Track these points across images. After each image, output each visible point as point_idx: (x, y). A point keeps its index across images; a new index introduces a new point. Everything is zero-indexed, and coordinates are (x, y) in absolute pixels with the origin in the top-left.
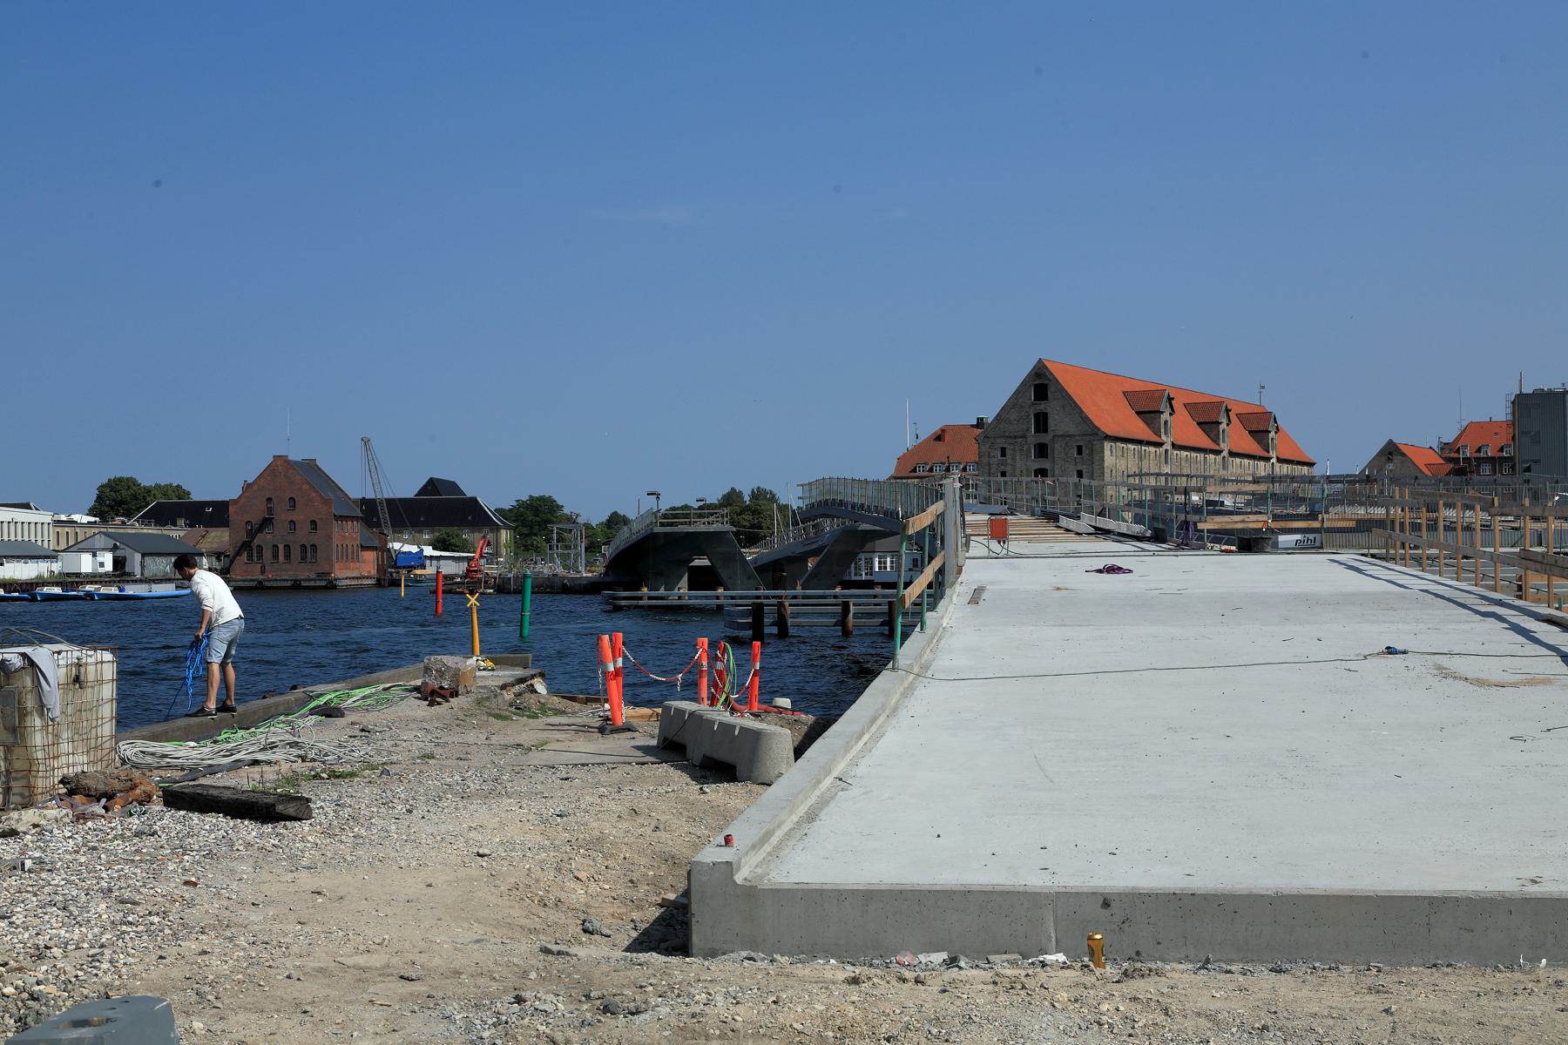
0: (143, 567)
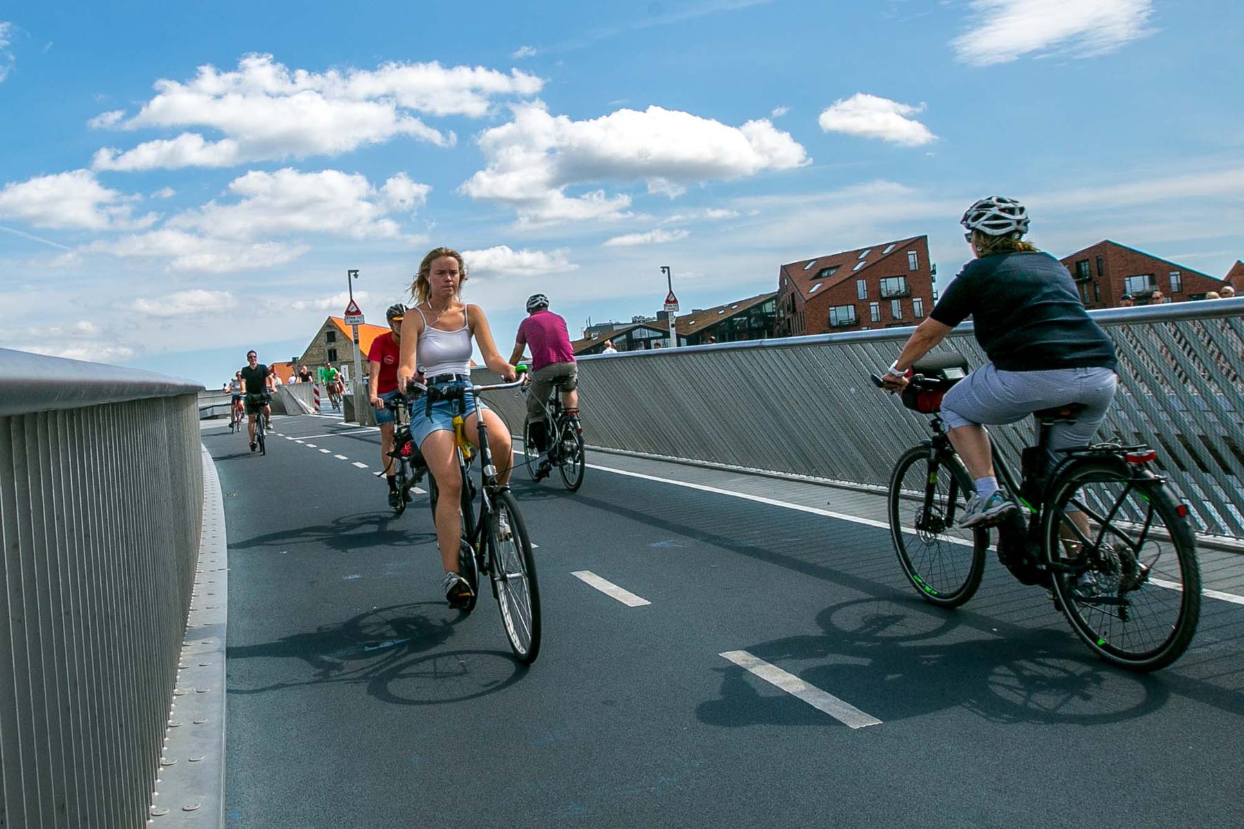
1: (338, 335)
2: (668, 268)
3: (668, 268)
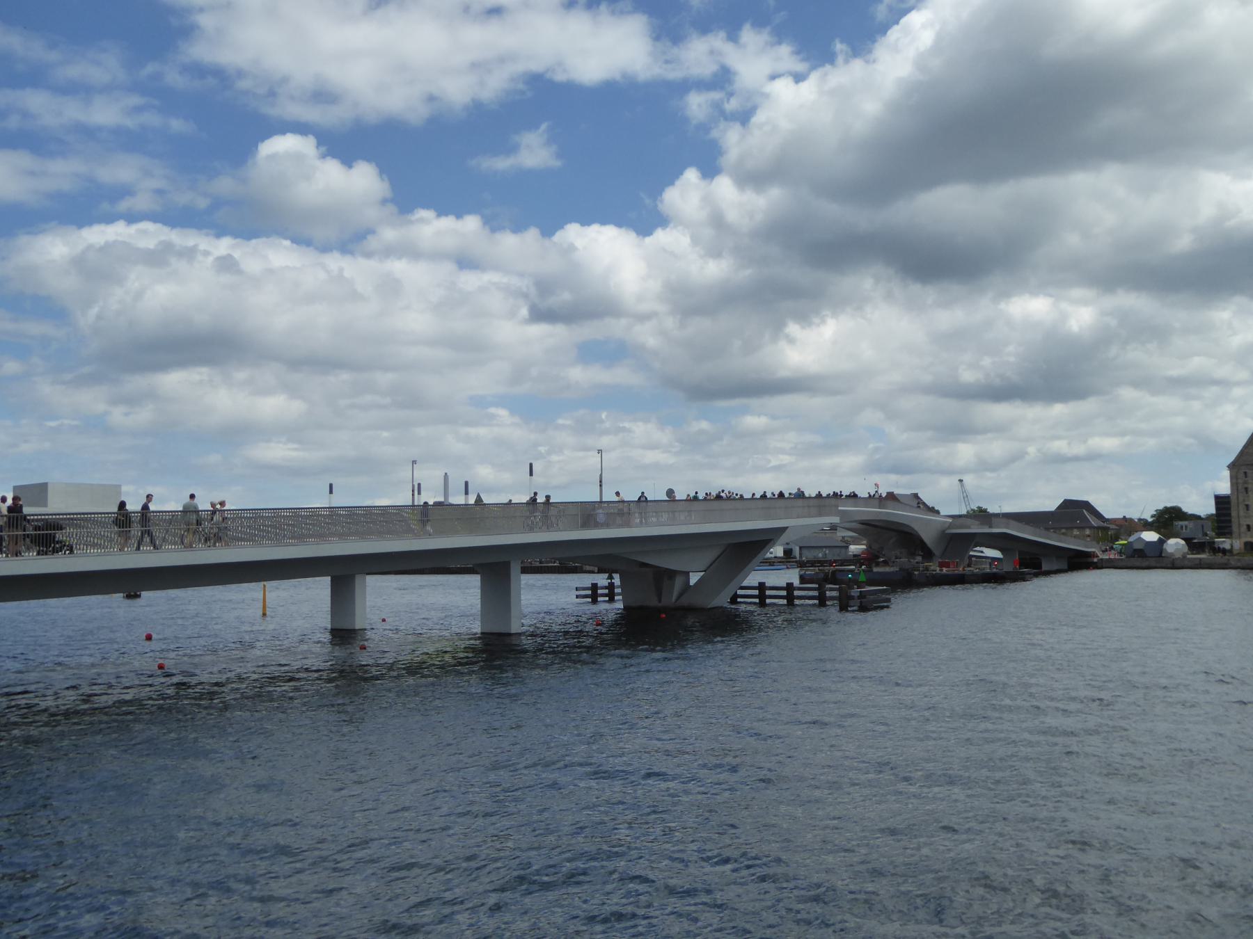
0: (800, 554)
2: (601, 450)
3: (601, 450)
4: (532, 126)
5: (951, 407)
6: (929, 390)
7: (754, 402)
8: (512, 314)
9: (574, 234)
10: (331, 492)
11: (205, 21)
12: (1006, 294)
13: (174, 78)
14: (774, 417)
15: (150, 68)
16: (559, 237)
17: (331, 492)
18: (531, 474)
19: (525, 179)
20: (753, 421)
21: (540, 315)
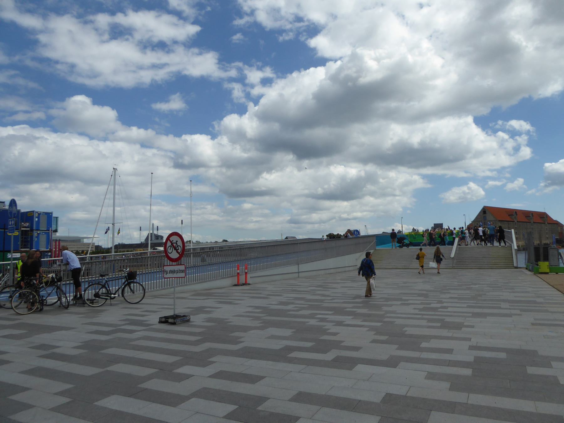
1: (487, 212)
4: (175, 93)
5: (311, 201)
6: (308, 196)
7: (247, 199)
8: (164, 165)
9: (184, 137)
10: (141, 230)
11: (43, 38)
12: (329, 164)
13: (29, 63)
14: (254, 204)
15: (17, 58)
16: (497, 134)
17: (141, 230)
18: (182, 224)
19: (171, 116)
20: (247, 206)
21: (178, 165)
